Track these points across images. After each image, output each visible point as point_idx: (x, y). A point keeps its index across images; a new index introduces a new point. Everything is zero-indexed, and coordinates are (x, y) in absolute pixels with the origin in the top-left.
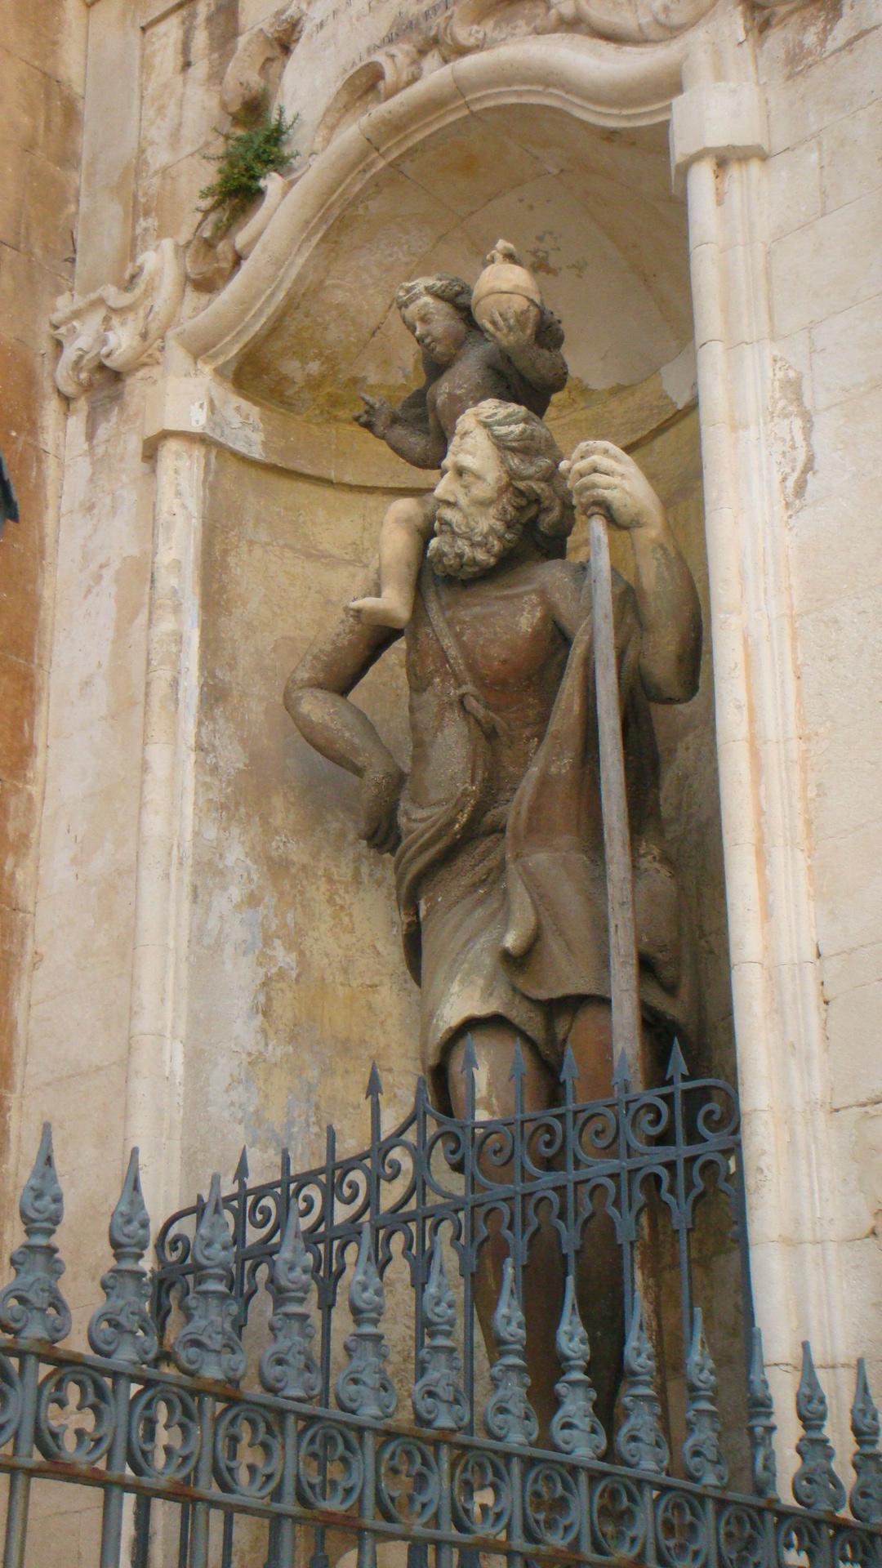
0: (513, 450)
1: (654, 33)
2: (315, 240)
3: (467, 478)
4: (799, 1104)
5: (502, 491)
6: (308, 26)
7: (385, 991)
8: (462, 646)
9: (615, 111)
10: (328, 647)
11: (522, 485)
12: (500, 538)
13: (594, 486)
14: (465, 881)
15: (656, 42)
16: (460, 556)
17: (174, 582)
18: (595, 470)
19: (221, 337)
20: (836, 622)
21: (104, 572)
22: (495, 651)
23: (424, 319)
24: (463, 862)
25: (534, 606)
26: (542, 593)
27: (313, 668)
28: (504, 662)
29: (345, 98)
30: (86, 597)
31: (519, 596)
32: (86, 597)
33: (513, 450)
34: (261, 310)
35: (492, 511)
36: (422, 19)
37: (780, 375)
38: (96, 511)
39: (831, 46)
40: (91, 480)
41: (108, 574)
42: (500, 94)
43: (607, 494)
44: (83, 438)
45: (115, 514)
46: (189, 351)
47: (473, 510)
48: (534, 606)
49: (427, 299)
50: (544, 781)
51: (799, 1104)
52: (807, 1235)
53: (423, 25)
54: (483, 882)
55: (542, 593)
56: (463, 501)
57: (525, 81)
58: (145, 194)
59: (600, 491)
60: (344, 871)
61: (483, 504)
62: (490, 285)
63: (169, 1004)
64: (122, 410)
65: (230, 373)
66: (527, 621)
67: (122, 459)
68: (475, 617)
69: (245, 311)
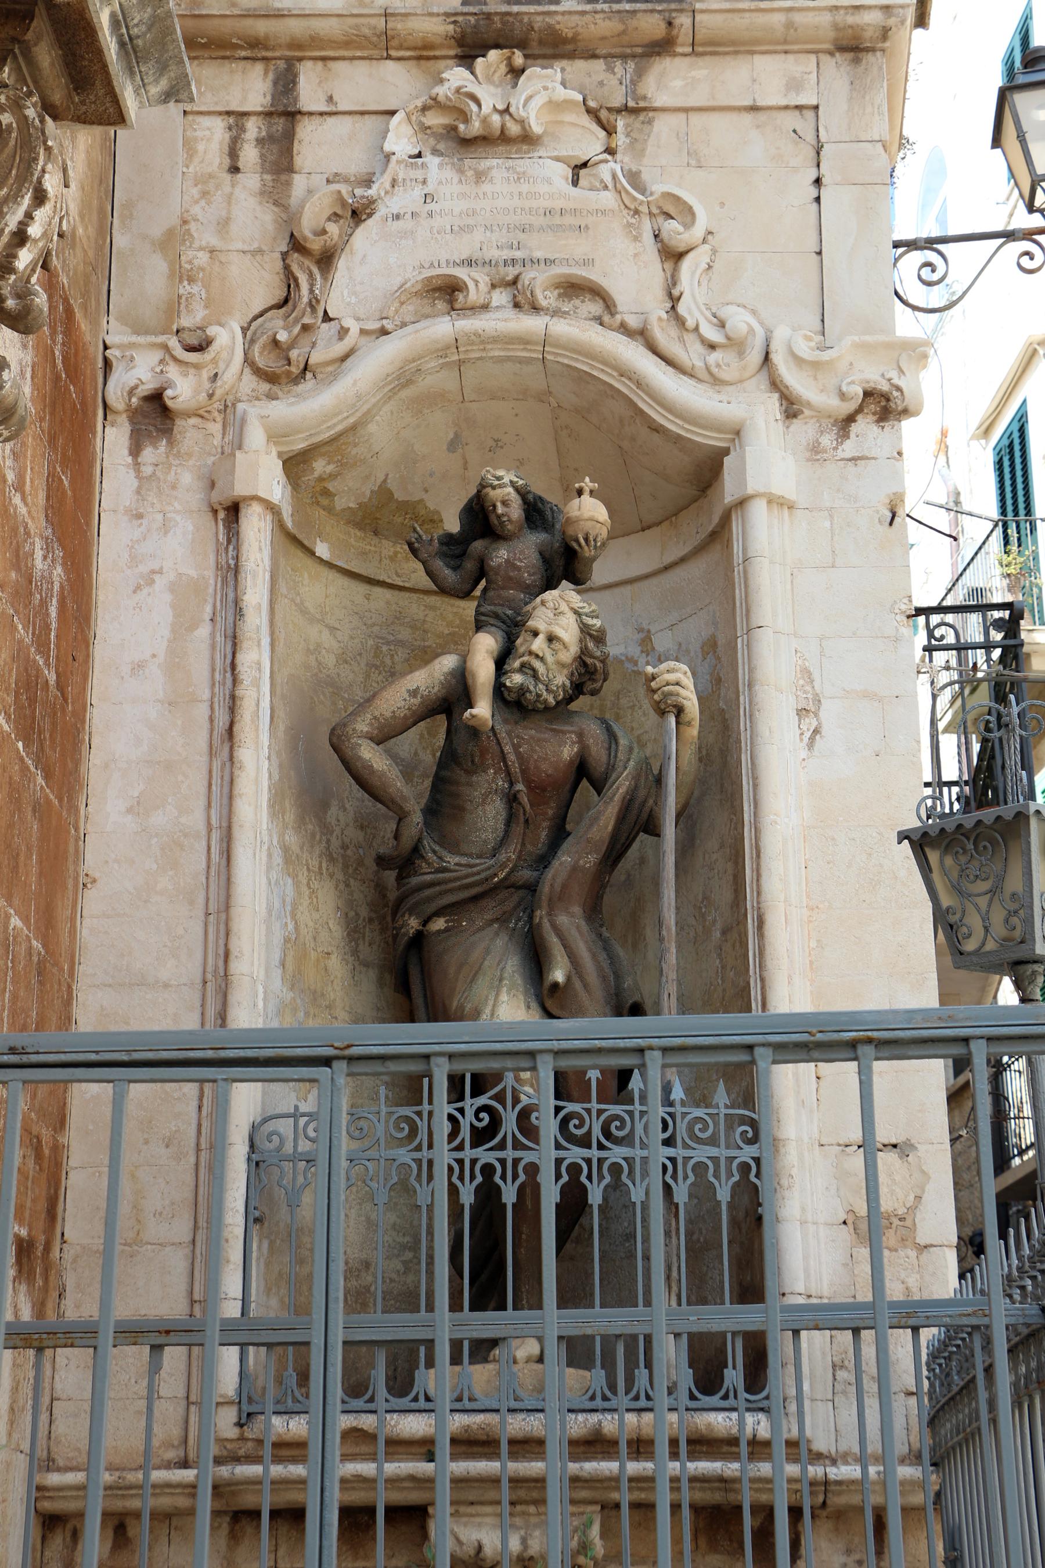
0: (591, 635)
1: (703, 374)
2: (386, 390)
3: (556, 645)
4: (806, 1140)
5: (575, 659)
6: (382, 211)
7: (333, 957)
8: (518, 755)
9: (595, 373)
10: (388, 714)
11: (589, 661)
12: (564, 691)
13: (678, 695)
14: (488, 916)
15: (700, 380)
16: (539, 696)
17: (258, 621)
18: (677, 684)
19: (299, 432)
20: (833, 839)
21: (156, 577)
22: (544, 766)
23: (505, 503)
24: (489, 903)
25: (573, 743)
26: (581, 735)
27: (371, 724)
28: (548, 776)
29: (419, 287)
30: (135, 592)
31: (564, 732)
32: (135, 592)
33: (591, 635)
34: (335, 425)
35: (565, 671)
36: (502, 264)
37: (800, 662)
38: (145, 521)
39: (840, 454)
40: (138, 492)
41: (160, 582)
42: (577, 360)
43: (685, 702)
44: (126, 452)
45: (166, 533)
46: (266, 431)
47: (554, 667)
48: (573, 743)
49: (510, 490)
50: (575, 869)
51: (806, 1140)
52: (810, 1219)
53: (501, 269)
54: (497, 920)
55: (581, 735)
56: (550, 659)
57: (605, 363)
58: (190, 262)
59: (680, 699)
60: (314, 863)
61: (562, 665)
62: (591, 514)
63: (256, 954)
64: (171, 443)
65: (285, 457)
66: (568, 752)
67: (174, 487)
68: (532, 737)
69: (324, 422)
